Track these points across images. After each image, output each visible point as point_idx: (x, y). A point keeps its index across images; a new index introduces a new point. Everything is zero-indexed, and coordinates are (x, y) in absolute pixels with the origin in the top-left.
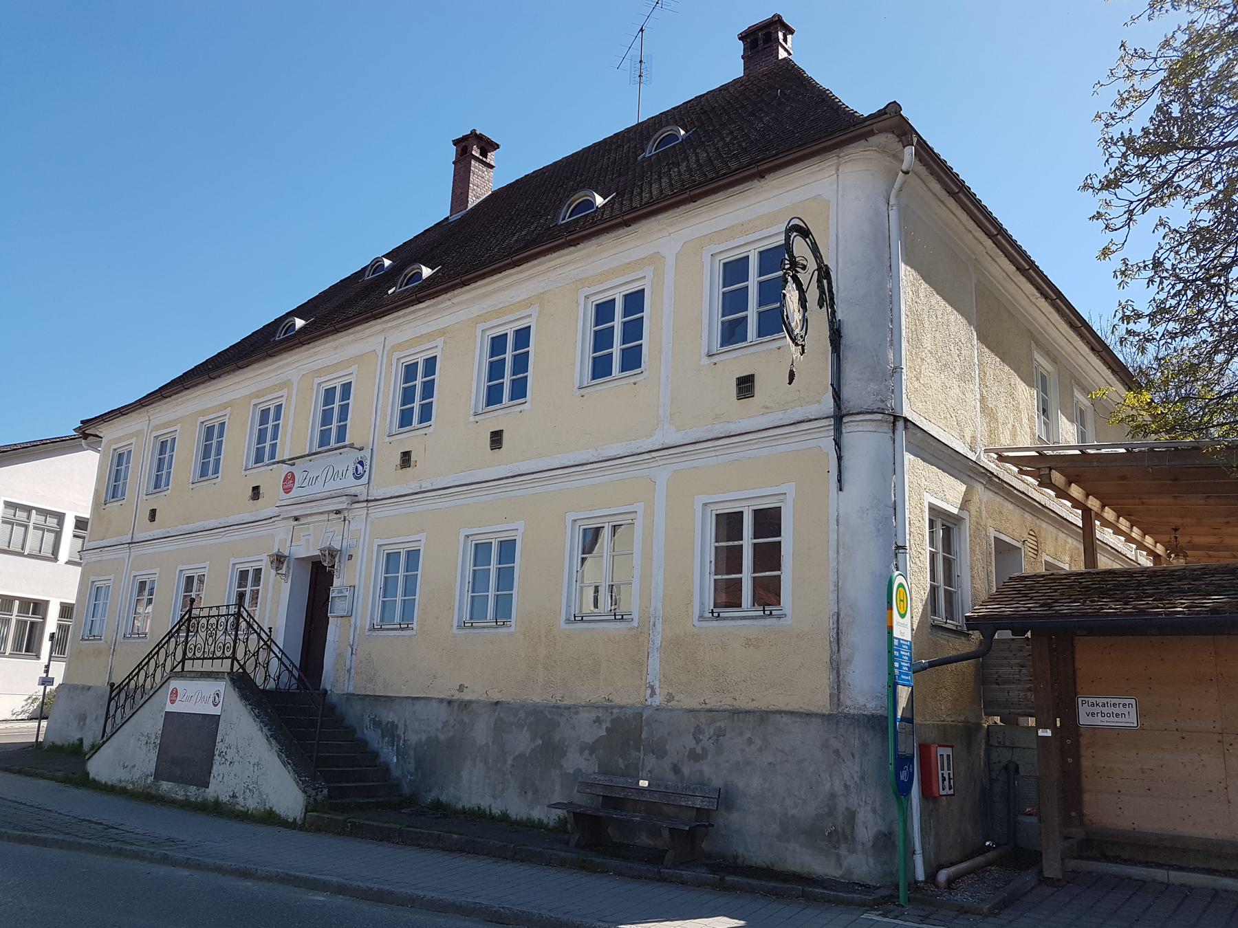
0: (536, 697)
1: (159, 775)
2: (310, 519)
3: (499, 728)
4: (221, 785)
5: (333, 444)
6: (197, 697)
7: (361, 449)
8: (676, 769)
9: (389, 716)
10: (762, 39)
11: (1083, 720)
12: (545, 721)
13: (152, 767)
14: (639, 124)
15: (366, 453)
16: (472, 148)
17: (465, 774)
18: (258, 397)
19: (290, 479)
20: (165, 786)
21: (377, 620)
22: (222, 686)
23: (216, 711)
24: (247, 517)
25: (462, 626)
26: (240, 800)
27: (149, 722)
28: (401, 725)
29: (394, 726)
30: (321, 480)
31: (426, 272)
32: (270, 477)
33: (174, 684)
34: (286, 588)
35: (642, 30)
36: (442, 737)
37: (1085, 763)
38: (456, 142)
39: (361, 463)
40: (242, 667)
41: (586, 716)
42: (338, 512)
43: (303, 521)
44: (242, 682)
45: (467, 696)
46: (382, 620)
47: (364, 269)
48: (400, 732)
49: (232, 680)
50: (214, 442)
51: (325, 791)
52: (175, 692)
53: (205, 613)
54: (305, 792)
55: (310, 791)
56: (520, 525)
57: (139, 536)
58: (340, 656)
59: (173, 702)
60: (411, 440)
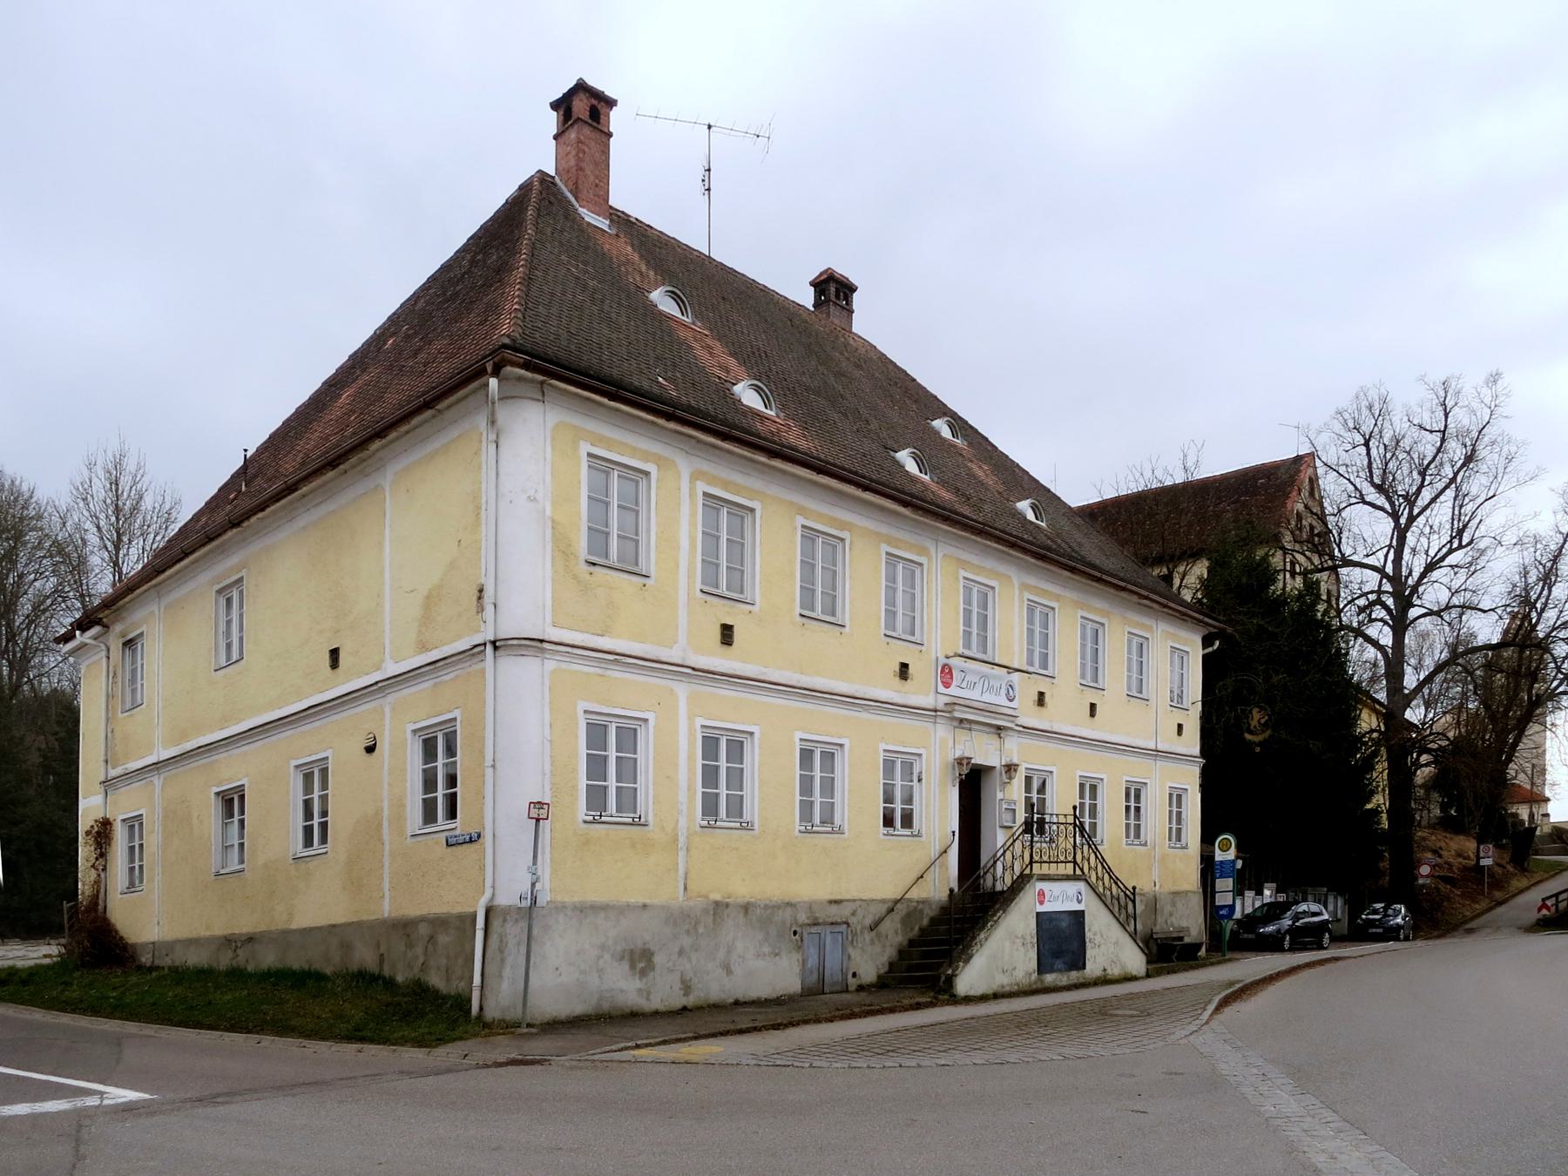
1: (1041, 969)
4: (1095, 963)
20: (1050, 978)
26: (1109, 971)
38: (555, 106)
42: (999, 728)
59: (1041, 903)
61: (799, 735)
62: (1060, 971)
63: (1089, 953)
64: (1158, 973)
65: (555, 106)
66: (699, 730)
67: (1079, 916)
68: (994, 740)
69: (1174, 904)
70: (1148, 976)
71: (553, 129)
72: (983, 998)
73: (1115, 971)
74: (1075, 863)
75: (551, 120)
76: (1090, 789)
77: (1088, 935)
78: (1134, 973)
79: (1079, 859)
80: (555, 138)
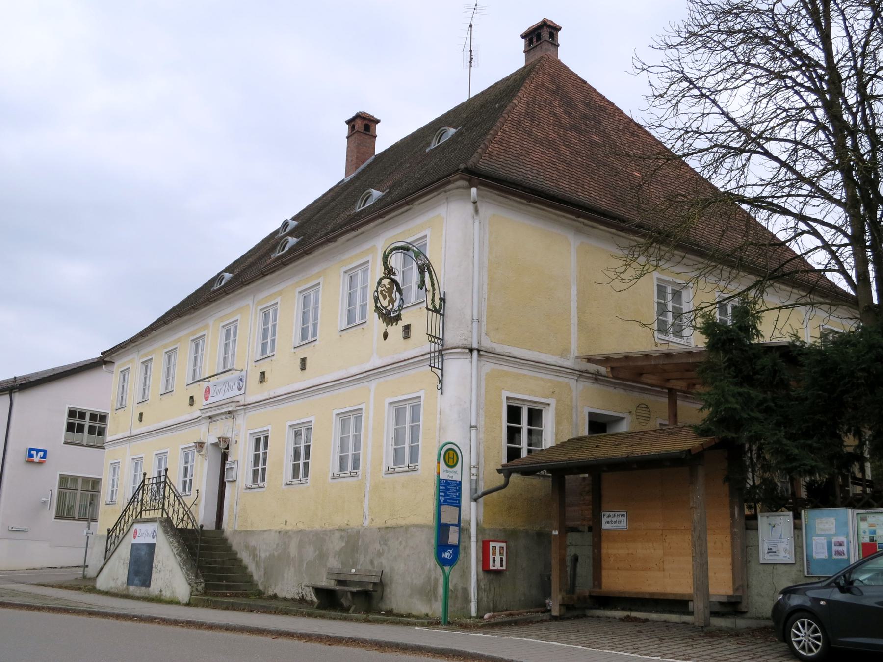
0: (317, 527)
1: (130, 582)
2: (218, 418)
3: (301, 546)
4: (157, 584)
5: (310, 339)
6: (147, 533)
7: (242, 371)
8: (372, 562)
9: (252, 542)
10: (542, 36)
11: (605, 526)
12: (319, 538)
13: (125, 578)
14: (470, 100)
15: (244, 373)
16: (362, 126)
17: (285, 575)
18: (193, 335)
19: (208, 391)
20: (132, 589)
21: (391, 465)
22: (156, 526)
23: (152, 541)
24: (187, 417)
25: (389, 472)
26: (164, 593)
27: (124, 552)
28: (258, 548)
29: (254, 549)
30: (223, 391)
31: (376, 194)
32: (198, 391)
33: (136, 526)
34: (206, 464)
35: (471, 26)
36: (276, 553)
37: (604, 551)
38: (348, 122)
39: (241, 380)
40: (167, 514)
41: (337, 534)
42: (230, 413)
43: (214, 419)
44: (167, 524)
45: (288, 527)
46: (395, 464)
47: (279, 229)
48: (257, 552)
49: (161, 522)
50: (270, 325)
51: (203, 584)
52: (136, 532)
53: (150, 482)
54: (190, 584)
55: (193, 584)
56: (312, 418)
57: (135, 432)
58: (231, 507)
59: (135, 538)
60: (264, 366)
61: (505, 394)
62: (136, 585)
63: (154, 576)
64: (207, 604)
65: (348, 122)
66: (504, 400)
67: (152, 547)
68: (230, 421)
69: (384, 541)
70: (188, 604)
71: (347, 135)
72: (106, 593)
73: (167, 594)
74: (163, 509)
75: (522, 43)
76: (161, 457)
77: (155, 562)
78: (180, 599)
79: (166, 507)
80: (525, 52)
